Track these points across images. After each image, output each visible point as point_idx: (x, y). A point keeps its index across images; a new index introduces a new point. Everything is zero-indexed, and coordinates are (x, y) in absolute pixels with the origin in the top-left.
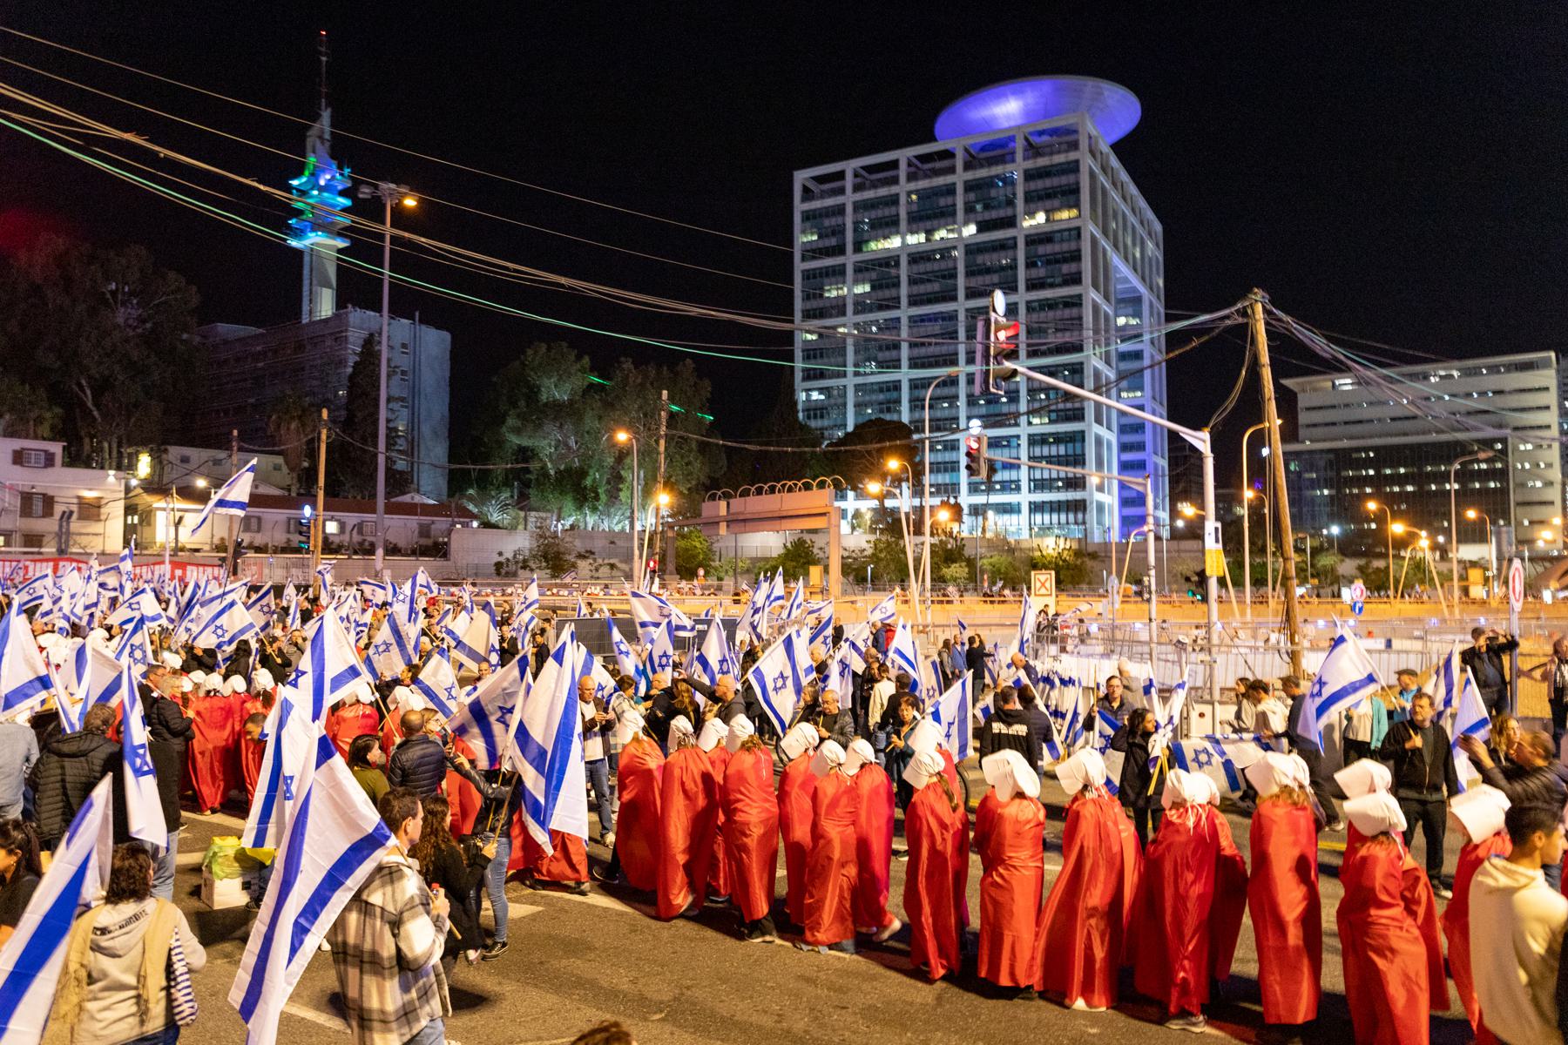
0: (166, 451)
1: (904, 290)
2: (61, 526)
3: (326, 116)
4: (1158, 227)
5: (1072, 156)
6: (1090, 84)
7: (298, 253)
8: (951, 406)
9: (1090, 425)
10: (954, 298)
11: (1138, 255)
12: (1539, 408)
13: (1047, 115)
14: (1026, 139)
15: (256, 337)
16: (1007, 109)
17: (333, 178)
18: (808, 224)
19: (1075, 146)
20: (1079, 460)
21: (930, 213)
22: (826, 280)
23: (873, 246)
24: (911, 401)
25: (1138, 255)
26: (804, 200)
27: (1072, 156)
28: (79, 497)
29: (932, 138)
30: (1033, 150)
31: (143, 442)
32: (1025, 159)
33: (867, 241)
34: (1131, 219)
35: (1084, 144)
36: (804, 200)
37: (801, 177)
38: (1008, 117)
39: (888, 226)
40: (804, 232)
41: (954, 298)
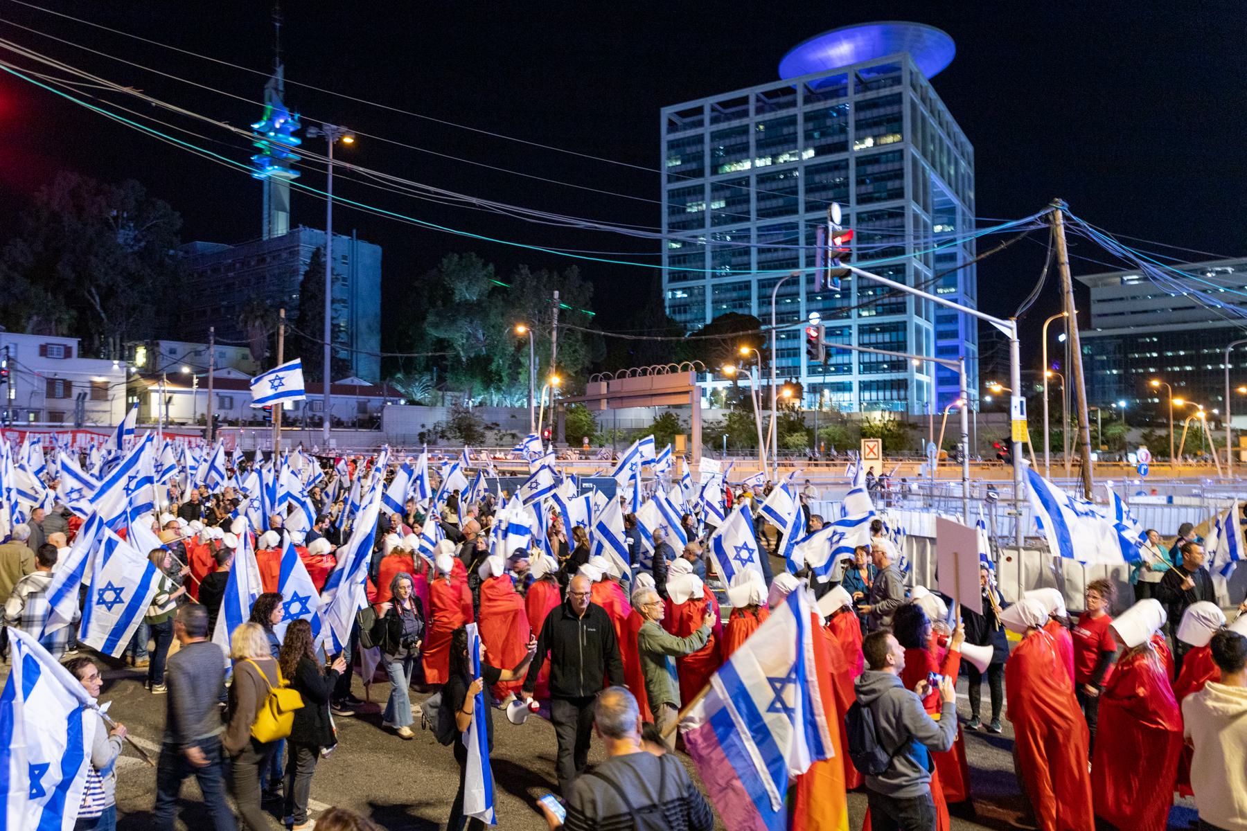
0: (158, 345)
1: (753, 205)
3: (280, 70)
4: (970, 148)
5: (896, 89)
10: (796, 212)
11: (952, 172)
14: (857, 76)
16: (841, 51)
17: (286, 122)
18: (673, 152)
20: (902, 346)
21: (775, 140)
22: (688, 198)
23: (727, 169)
24: (759, 298)
25: (952, 172)
27: (896, 89)
29: (777, 78)
30: (862, 85)
33: (723, 165)
34: (947, 141)
35: (906, 79)
36: (670, 131)
37: (667, 112)
38: (841, 58)
39: (740, 152)
40: (669, 158)
41: (796, 212)
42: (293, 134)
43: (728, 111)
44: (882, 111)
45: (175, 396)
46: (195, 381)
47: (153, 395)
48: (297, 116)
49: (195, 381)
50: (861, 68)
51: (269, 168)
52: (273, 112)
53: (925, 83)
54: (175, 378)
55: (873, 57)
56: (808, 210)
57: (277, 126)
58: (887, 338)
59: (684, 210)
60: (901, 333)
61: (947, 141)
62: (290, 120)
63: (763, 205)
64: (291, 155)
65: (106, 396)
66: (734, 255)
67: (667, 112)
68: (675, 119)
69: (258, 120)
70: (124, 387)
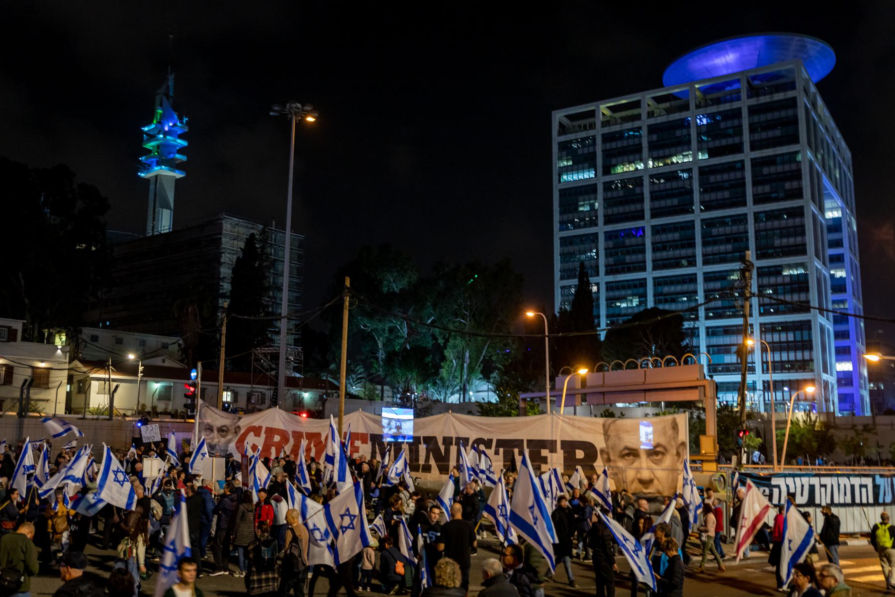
0: (81, 332)
1: (647, 205)
2: (22, 393)
4: (848, 154)
5: (790, 94)
6: (795, 40)
7: (147, 181)
8: (689, 300)
9: (815, 316)
11: (838, 176)
12: (43, 400)
13: (760, 63)
14: (748, 83)
15: (830, 177)
16: (725, 60)
17: (175, 125)
18: (564, 153)
19: (792, 86)
20: (807, 345)
22: (581, 198)
23: (619, 169)
24: (655, 296)
25: (838, 176)
26: (560, 134)
27: (790, 94)
28: (33, 368)
30: (753, 92)
31: (61, 325)
32: (749, 97)
33: (615, 165)
34: (833, 148)
35: (799, 85)
36: (560, 134)
37: (558, 116)
38: (727, 66)
39: (633, 153)
40: (560, 159)
42: (180, 137)
43: (576, 123)
44: (776, 115)
45: (122, 385)
46: (141, 368)
47: (93, 382)
48: (185, 120)
49: (141, 368)
50: (753, 74)
51: (157, 168)
52: (162, 116)
53: (813, 89)
54: (121, 367)
55: (758, 65)
56: (653, 216)
57: (166, 129)
58: (791, 337)
59: (576, 209)
60: (805, 333)
61: (833, 148)
62: (179, 124)
63: (657, 204)
64: (178, 156)
65: (47, 383)
66: (628, 253)
67: (558, 116)
68: (566, 121)
69: (149, 123)
70: (66, 373)
